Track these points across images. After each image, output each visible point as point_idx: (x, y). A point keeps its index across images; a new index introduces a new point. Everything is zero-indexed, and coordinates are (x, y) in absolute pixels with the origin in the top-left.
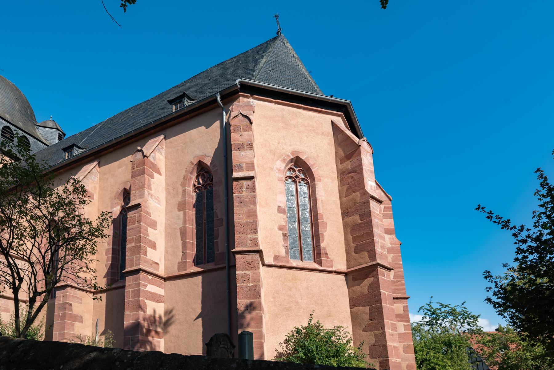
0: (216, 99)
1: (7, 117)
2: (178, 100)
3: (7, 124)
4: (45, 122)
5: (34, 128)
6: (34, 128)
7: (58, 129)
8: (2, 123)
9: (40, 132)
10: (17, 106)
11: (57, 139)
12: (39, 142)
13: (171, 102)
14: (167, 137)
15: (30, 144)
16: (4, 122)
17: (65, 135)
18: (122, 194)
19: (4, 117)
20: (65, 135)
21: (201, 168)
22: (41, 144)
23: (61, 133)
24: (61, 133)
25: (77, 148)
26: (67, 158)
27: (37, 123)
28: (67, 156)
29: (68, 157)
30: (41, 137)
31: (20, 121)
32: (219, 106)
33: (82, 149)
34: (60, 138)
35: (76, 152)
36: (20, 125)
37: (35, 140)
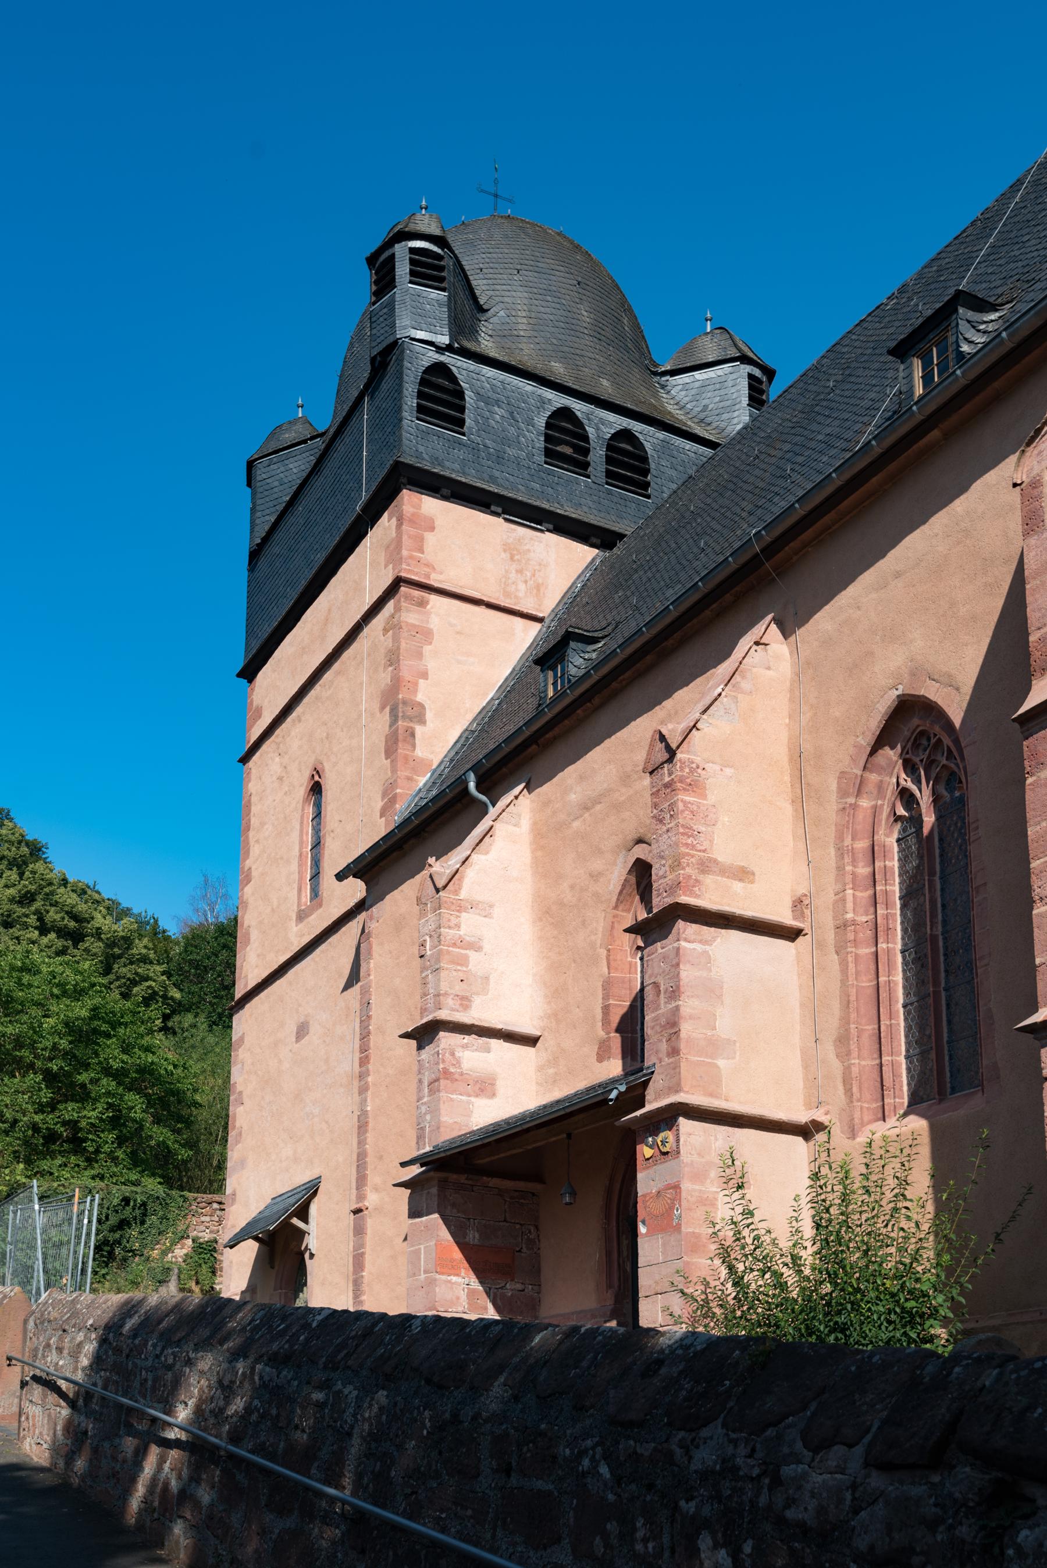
0: (466, 789)
1: (558, 370)
2: (924, 336)
3: (558, 400)
4: (689, 349)
5: (650, 387)
6: (650, 387)
7: (744, 359)
8: (543, 402)
9: (680, 394)
10: (585, 316)
11: (745, 401)
12: (678, 441)
13: (902, 351)
14: (532, 785)
15: (644, 459)
16: (549, 394)
17: (770, 373)
18: (633, 879)
19: (547, 375)
20: (770, 373)
21: (911, 727)
22: (688, 445)
23: (757, 373)
24: (757, 373)
25: (970, 315)
26: (919, 390)
27: (656, 365)
28: (918, 373)
29: (927, 378)
30: (679, 414)
31: (602, 373)
32: (474, 800)
33: (994, 308)
34: (756, 396)
35: (971, 334)
36: (605, 388)
37: (662, 435)
